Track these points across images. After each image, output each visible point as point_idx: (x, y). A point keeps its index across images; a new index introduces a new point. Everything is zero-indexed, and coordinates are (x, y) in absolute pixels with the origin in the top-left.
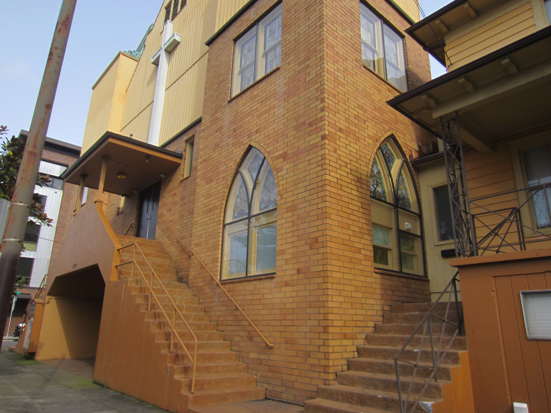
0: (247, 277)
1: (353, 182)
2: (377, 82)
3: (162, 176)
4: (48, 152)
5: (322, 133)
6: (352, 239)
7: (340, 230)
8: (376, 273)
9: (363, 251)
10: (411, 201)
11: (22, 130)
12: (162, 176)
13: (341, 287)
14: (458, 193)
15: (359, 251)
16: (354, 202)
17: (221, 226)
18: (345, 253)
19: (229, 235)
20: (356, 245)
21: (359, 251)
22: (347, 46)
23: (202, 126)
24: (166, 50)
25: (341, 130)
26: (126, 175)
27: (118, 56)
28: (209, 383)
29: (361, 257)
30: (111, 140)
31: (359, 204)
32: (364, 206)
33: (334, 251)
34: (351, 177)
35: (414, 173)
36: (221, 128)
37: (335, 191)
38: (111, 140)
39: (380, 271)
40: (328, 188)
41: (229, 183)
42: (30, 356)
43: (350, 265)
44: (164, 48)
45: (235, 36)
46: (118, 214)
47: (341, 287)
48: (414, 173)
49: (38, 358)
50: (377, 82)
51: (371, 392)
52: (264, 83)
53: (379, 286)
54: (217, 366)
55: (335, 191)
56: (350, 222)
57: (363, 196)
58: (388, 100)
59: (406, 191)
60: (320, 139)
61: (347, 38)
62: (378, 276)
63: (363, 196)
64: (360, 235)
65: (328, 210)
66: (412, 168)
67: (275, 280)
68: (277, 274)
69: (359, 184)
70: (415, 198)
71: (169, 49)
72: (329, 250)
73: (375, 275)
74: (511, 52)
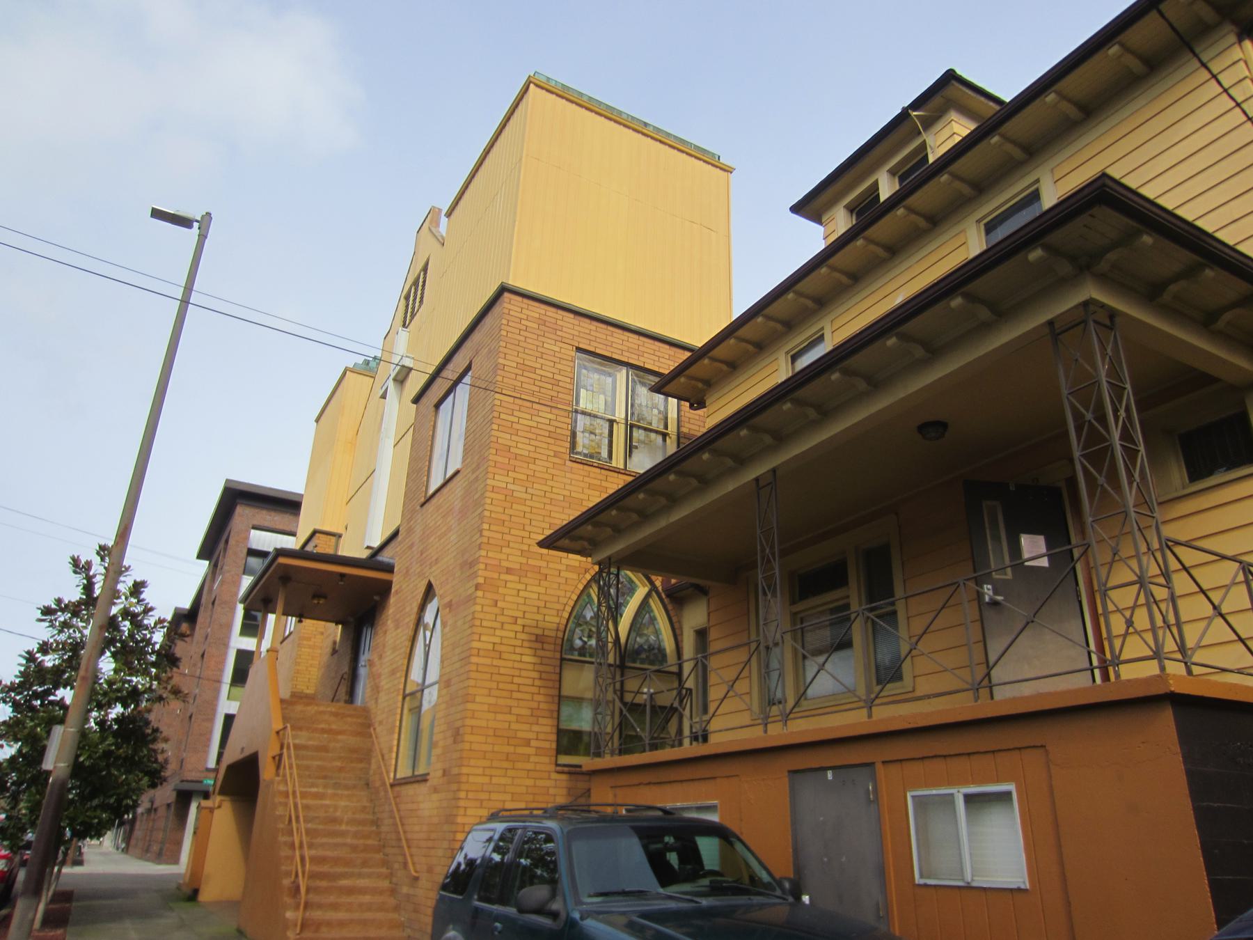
0: (414, 776)
1: (526, 644)
2: (600, 477)
3: (376, 598)
4: (273, 514)
5: (475, 582)
6: (514, 726)
7: (491, 716)
8: (558, 772)
9: (533, 743)
10: (668, 651)
11: (227, 481)
12: (376, 598)
13: (483, 796)
14: (989, 566)
15: (527, 743)
16: (524, 673)
17: (400, 698)
18: (497, 748)
19: (410, 710)
20: (520, 735)
21: (527, 743)
22: (540, 438)
23: (400, 538)
24: (395, 380)
25: (509, 571)
26: (325, 597)
27: (344, 374)
28: (329, 924)
29: (531, 751)
30: (282, 560)
31: (536, 675)
32: (544, 676)
33: (475, 747)
34: (524, 636)
35: (670, 607)
36: (412, 545)
37: (488, 661)
38: (282, 560)
39: (566, 769)
40: (474, 659)
41: (411, 633)
42: (193, 896)
43: (506, 764)
44: (393, 376)
45: (435, 400)
46: (334, 652)
47: (483, 796)
48: (670, 607)
49: (204, 897)
50: (600, 477)
51: (368, 915)
52: (445, 490)
53: (564, 792)
54: (350, 904)
55: (488, 661)
56: (514, 703)
57: (545, 661)
58: (541, 537)
59: (657, 637)
60: (473, 589)
61: (540, 426)
62: (564, 777)
63: (545, 661)
64: (532, 720)
65: (471, 691)
66: (666, 601)
67: (428, 784)
68: (432, 775)
69: (539, 645)
70: (673, 646)
71: (400, 378)
72: (467, 746)
73: (554, 776)
74: (617, 501)
